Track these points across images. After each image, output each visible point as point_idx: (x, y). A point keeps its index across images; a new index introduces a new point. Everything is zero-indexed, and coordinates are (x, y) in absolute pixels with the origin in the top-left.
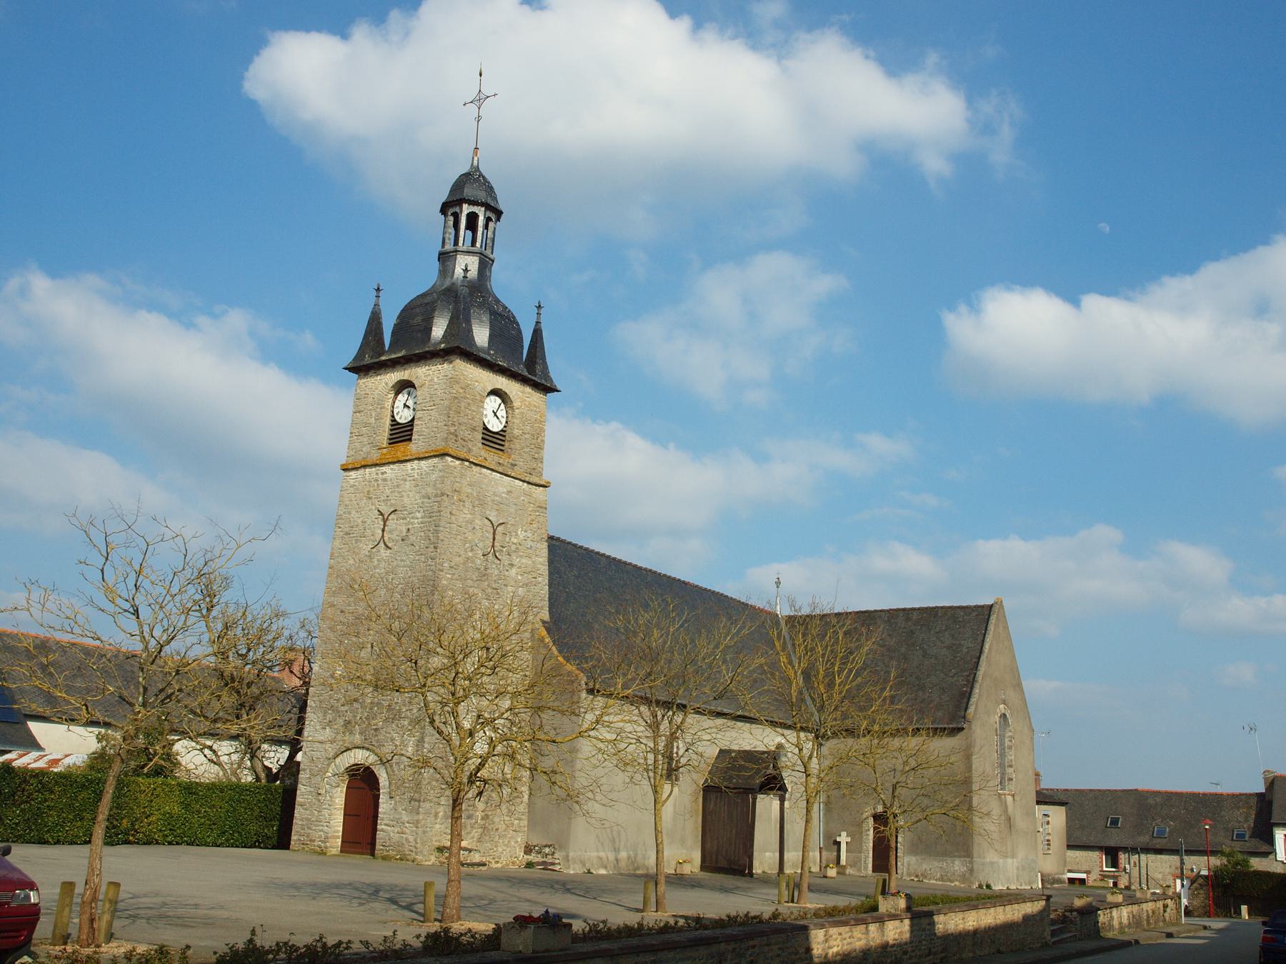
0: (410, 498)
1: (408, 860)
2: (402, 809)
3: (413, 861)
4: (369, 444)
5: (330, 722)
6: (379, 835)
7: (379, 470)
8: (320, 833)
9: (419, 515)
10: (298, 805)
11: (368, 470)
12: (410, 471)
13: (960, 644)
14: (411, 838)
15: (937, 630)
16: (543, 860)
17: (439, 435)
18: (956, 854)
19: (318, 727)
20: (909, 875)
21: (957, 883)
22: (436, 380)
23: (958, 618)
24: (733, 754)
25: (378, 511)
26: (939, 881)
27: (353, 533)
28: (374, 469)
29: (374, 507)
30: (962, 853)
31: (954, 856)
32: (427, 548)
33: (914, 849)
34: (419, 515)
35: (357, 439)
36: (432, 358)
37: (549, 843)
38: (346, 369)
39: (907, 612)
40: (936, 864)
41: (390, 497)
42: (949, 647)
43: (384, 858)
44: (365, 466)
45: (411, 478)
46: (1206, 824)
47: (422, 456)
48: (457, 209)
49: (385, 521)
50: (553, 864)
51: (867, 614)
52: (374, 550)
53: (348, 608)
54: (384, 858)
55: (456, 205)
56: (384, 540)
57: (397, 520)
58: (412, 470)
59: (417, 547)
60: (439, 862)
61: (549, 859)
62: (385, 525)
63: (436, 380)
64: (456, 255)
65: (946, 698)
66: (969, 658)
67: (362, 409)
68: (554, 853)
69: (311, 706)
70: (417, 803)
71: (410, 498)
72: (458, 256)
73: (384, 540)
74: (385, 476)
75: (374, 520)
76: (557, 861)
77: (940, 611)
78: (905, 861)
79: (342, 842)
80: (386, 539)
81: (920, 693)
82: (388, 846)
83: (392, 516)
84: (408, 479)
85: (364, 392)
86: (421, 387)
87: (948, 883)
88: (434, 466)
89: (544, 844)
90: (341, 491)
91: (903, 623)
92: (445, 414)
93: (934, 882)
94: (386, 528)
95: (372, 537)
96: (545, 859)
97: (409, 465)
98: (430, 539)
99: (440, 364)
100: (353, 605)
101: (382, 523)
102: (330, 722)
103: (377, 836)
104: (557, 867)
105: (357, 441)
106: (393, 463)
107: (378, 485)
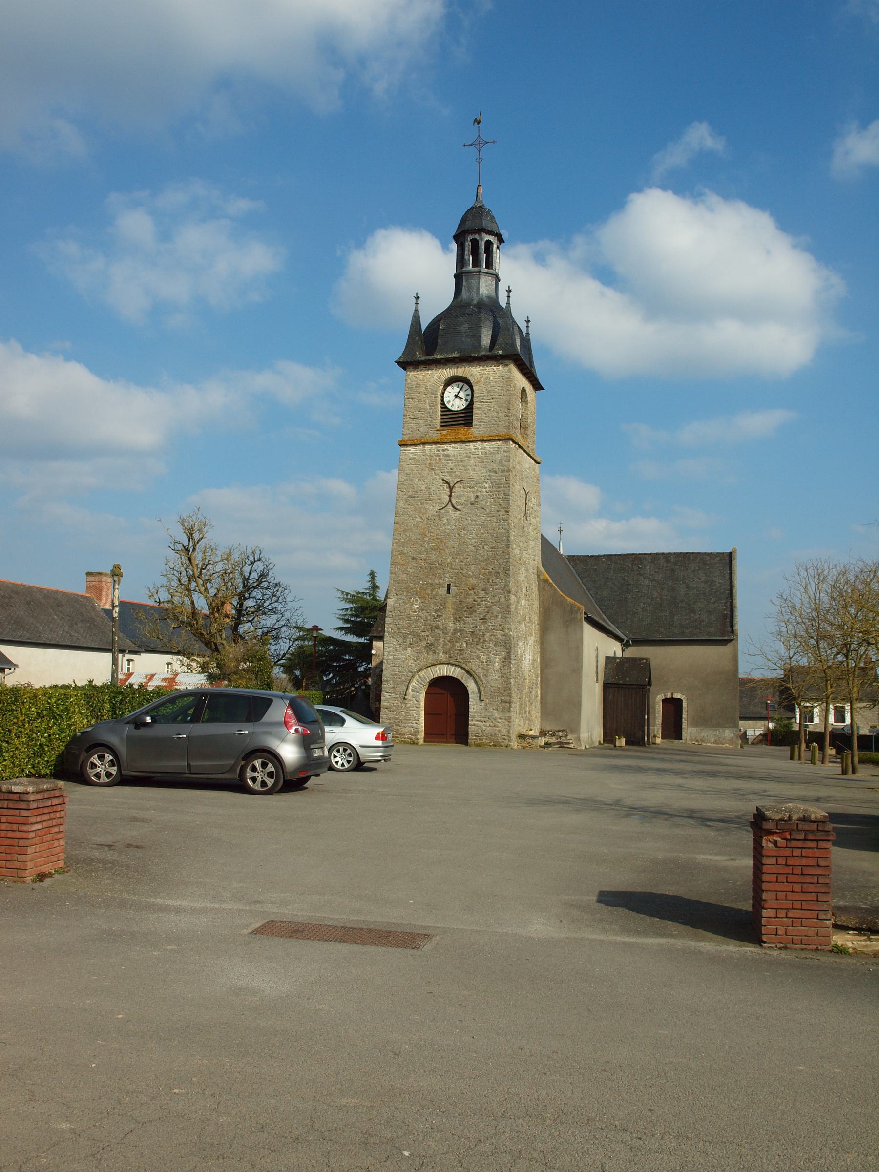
0: (476, 472)
1: (502, 746)
2: (493, 709)
3: (507, 747)
4: (426, 425)
5: (410, 644)
6: (471, 729)
7: (440, 447)
8: (409, 729)
9: (487, 486)
10: (383, 708)
11: (427, 447)
12: (473, 450)
13: (713, 580)
14: (504, 730)
15: (693, 570)
16: (557, 741)
17: (500, 423)
18: (727, 725)
19: (398, 648)
20: (691, 740)
21: (727, 745)
22: (492, 378)
23: (706, 561)
24: (618, 660)
25: (443, 480)
26: (714, 743)
27: (418, 497)
28: (434, 446)
29: (438, 477)
30: (731, 725)
31: (725, 727)
32: (497, 511)
33: (695, 723)
34: (487, 486)
35: (413, 421)
36: (486, 361)
37: (562, 729)
38: (396, 362)
39: (666, 556)
40: (711, 732)
41: (455, 470)
42: (706, 582)
43: (478, 745)
44: (424, 444)
45: (476, 456)
46: (768, 700)
47: (485, 439)
48: (477, 237)
49: (451, 489)
50: (569, 743)
51: (634, 556)
52: (443, 511)
53: (420, 556)
54: (478, 745)
55: (475, 233)
56: (452, 504)
57: (464, 488)
58: (475, 449)
59: (488, 511)
60: (522, 746)
61: (563, 740)
62: (451, 492)
63: (492, 378)
64: (479, 275)
65: (713, 618)
66: (723, 591)
67: (416, 397)
68: (566, 736)
69: (388, 632)
70: (508, 705)
71: (476, 472)
72: (481, 276)
73: (452, 504)
74: (446, 452)
75: (439, 487)
76: (571, 741)
77: (691, 556)
78: (688, 731)
79: (425, 734)
80: (454, 502)
81: (692, 615)
82: (480, 737)
83: (458, 484)
84: (472, 456)
85: (416, 383)
86: (477, 383)
87: (720, 745)
88: (498, 448)
89: (557, 729)
90: (400, 462)
91: (665, 563)
92: (505, 407)
93: (710, 744)
94: (453, 494)
95: (438, 501)
96: (559, 740)
97: (472, 445)
98: (500, 505)
99: (495, 366)
100: (425, 553)
101: (448, 490)
102: (410, 644)
103: (469, 729)
104: (572, 746)
105: (412, 422)
106: (455, 442)
107: (440, 459)
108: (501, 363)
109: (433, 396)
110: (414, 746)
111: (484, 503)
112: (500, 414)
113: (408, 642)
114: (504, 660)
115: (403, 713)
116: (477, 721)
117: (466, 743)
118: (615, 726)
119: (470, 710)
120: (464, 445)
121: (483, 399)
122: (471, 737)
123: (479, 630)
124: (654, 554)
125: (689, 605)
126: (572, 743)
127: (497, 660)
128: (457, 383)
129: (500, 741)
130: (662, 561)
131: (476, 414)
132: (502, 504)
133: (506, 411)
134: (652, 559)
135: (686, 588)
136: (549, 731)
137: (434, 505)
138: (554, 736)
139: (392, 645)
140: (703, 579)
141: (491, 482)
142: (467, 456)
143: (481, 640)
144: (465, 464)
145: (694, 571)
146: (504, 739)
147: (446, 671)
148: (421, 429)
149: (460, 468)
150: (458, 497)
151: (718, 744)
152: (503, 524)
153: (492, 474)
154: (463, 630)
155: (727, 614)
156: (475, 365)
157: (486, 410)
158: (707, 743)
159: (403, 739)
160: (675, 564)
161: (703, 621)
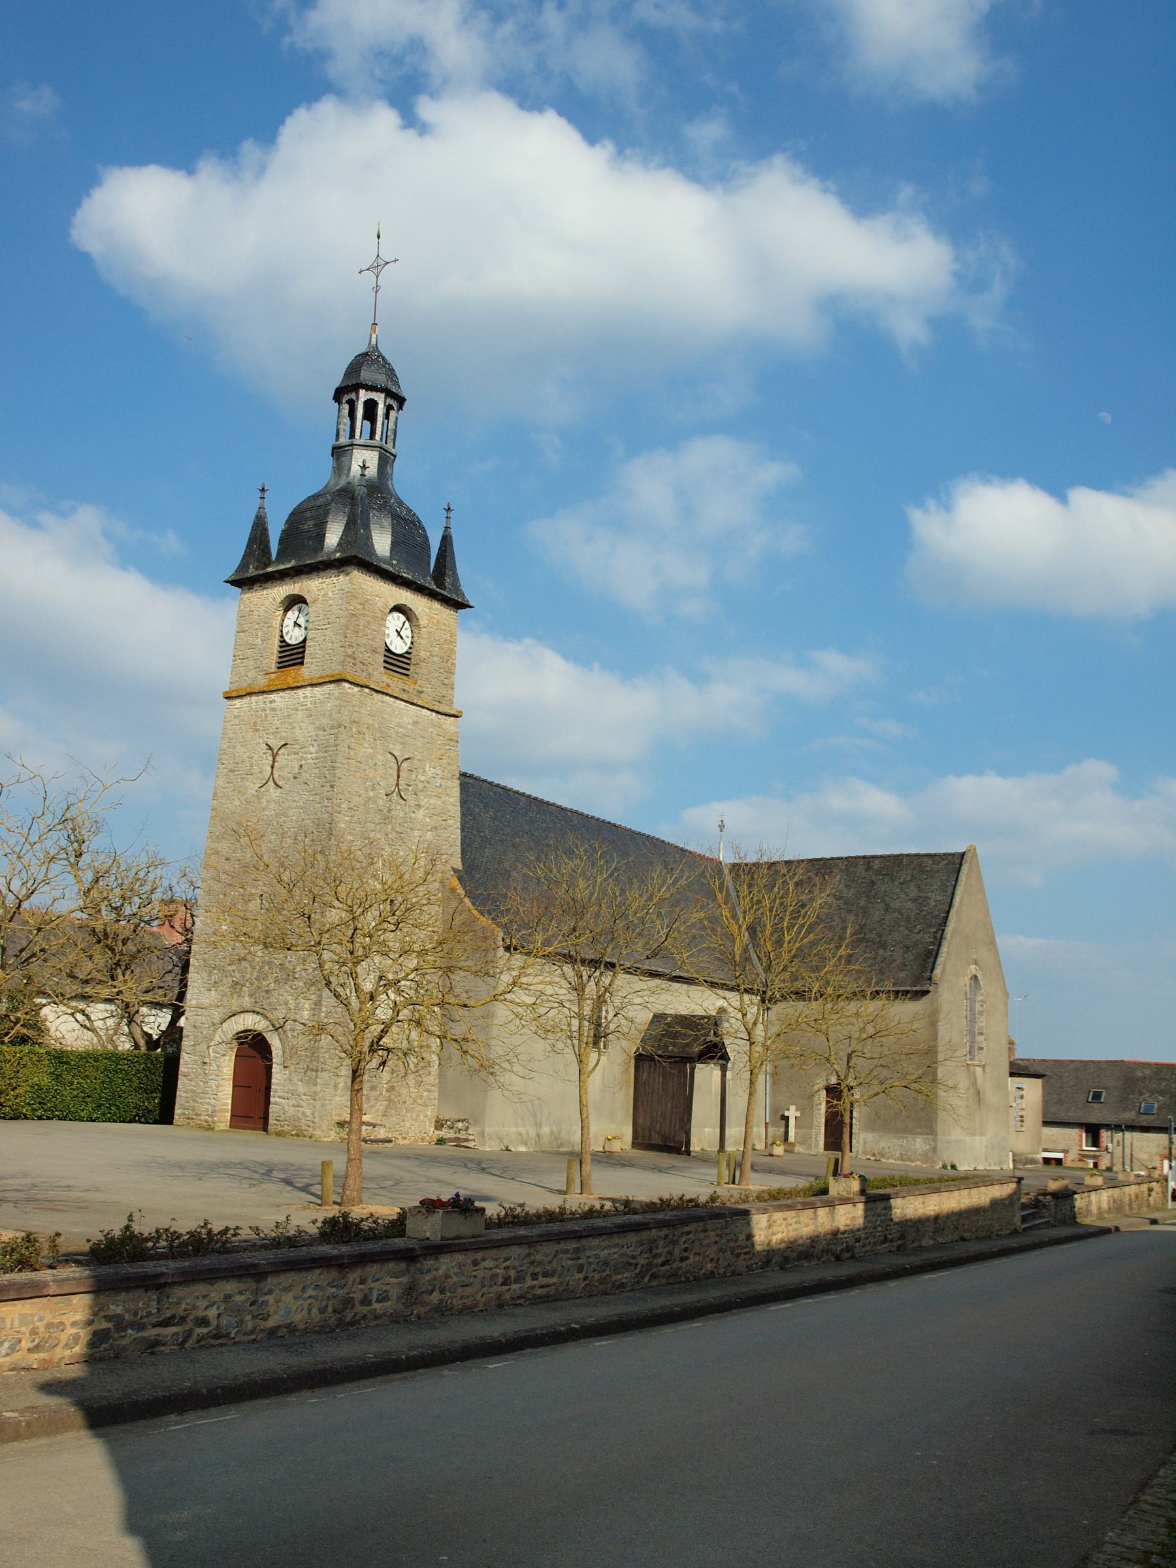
0: (303, 730)
3: (311, 1137)
4: (255, 668)
5: (215, 983)
7: (267, 698)
9: (313, 750)
13: (927, 897)
15: (901, 881)
16: (455, 1136)
17: (334, 658)
18: (918, 1130)
20: (865, 1153)
25: (267, 744)
26: (898, 1159)
27: (239, 771)
28: (261, 697)
29: (261, 741)
31: (916, 1134)
33: (870, 1126)
34: (313, 750)
35: (242, 663)
36: (326, 570)
37: (463, 1118)
38: (227, 582)
40: (895, 1141)
43: (278, 1134)
44: (250, 694)
45: (304, 708)
47: (315, 682)
48: (353, 396)
49: (274, 756)
50: (467, 1140)
51: (822, 862)
52: (263, 789)
53: (234, 855)
54: (278, 1134)
55: (351, 391)
59: (312, 786)
60: (340, 1138)
61: (463, 1135)
62: (274, 761)
63: (330, 594)
65: (910, 956)
69: (194, 966)
70: (314, 1073)
71: (303, 730)
72: (354, 451)
74: (273, 705)
76: (471, 1137)
78: (861, 1138)
79: (232, 1116)
80: (276, 776)
81: (881, 952)
83: (283, 750)
84: (300, 708)
85: (249, 609)
86: (313, 602)
87: (909, 1163)
88: (329, 694)
89: (457, 1118)
93: (893, 1161)
94: (276, 764)
95: (260, 775)
96: (457, 1135)
97: (300, 692)
101: (271, 759)
103: (270, 1110)
104: (471, 1144)
105: (241, 665)
108: (343, 571)
109: (266, 625)
110: (209, 1134)
111: (308, 776)
112: (336, 645)
113: (213, 980)
114: (313, 1006)
115: (202, 1083)
116: (280, 1097)
117: (264, 1126)
118: (648, 1123)
119: (273, 1081)
120: (292, 693)
121: (319, 625)
122: (272, 1121)
123: (290, 962)
124: (851, 857)
125: (881, 936)
126: (474, 1140)
127: (307, 1006)
128: (297, 606)
129: (304, 1128)
130: (860, 869)
131: (309, 646)
132: (327, 776)
133: (343, 639)
134: (846, 865)
135: (884, 910)
136: (446, 1121)
137: (254, 781)
138: (453, 1128)
139: (196, 984)
140: (912, 895)
141: (318, 745)
142: (293, 709)
143: (291, 978)
144: (291, 721)
145: (903, 883)
146: (309, 1126)
147: (249, 1022)
148: (250, 674)
149: (287, 726)
150: (281, 768)
151: (904, 1161)
152: (327, 804)
153: (320, 732)
154: (272, 962)
155: (933, 949)
156: (314, 577)
157: (320, 640)
158: (888, 1159)
159: (199, 1122)
160: (878, 872)
161: (894, 961)
